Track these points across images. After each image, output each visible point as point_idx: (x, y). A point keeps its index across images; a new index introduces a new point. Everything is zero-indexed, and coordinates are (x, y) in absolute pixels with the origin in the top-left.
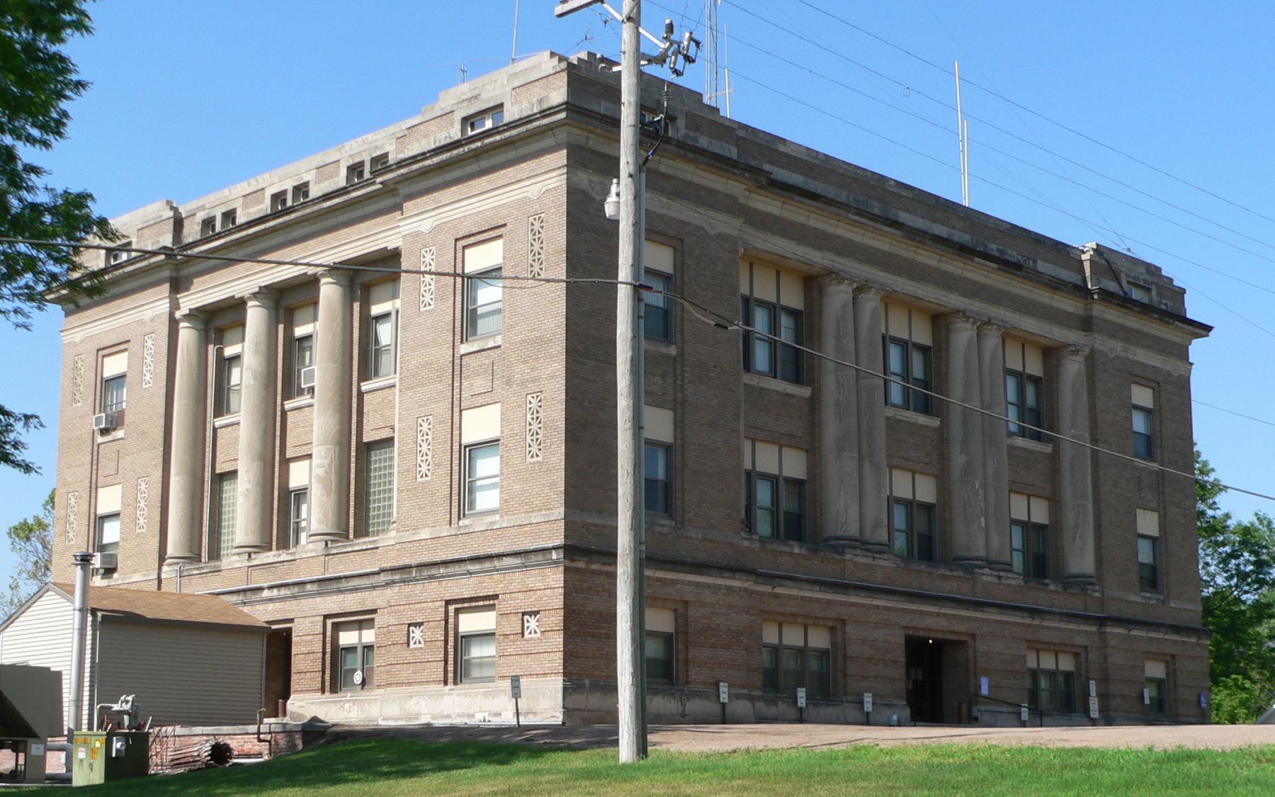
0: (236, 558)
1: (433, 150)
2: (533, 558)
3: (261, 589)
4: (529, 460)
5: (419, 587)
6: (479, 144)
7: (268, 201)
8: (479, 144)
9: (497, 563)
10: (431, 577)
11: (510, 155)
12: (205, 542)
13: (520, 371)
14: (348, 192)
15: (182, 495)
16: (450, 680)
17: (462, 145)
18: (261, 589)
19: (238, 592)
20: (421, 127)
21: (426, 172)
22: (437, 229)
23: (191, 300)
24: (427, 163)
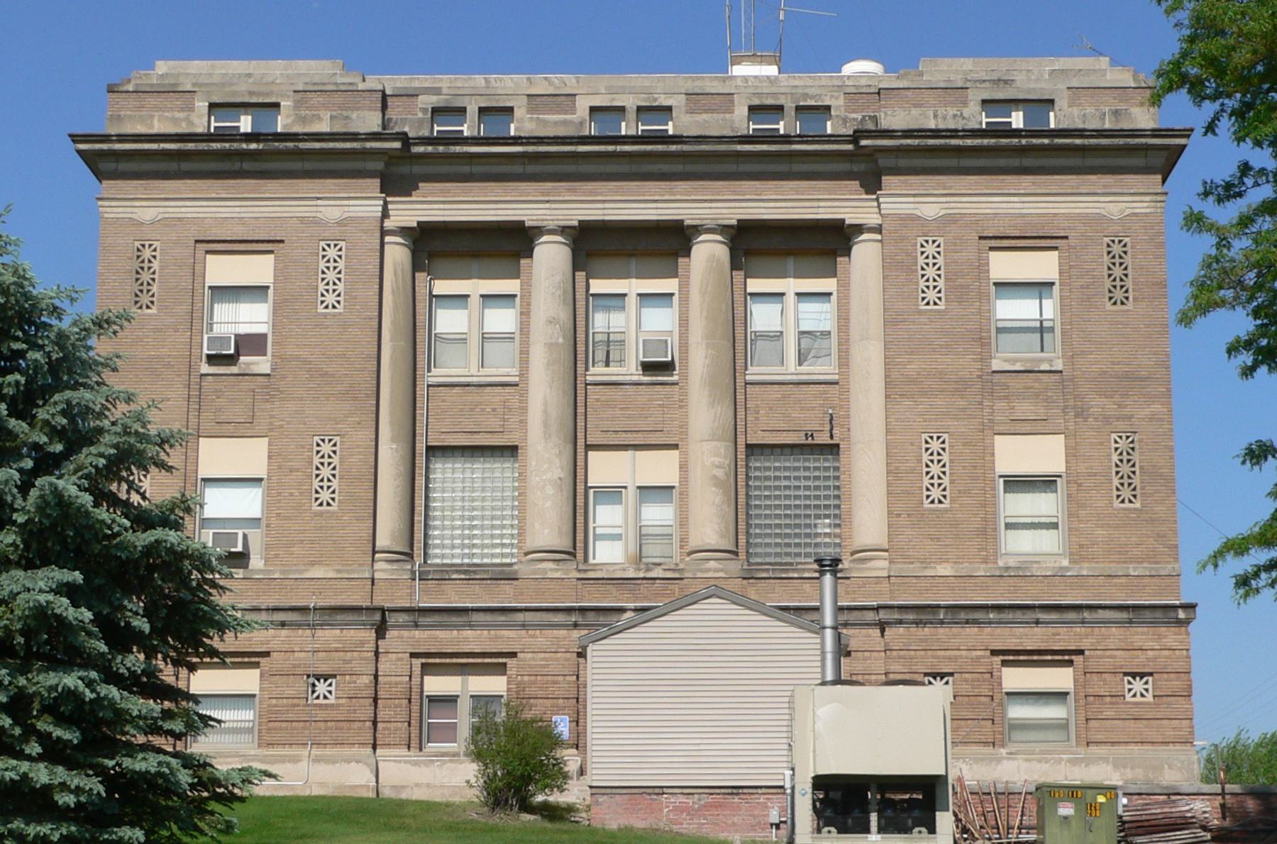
0: (551, 565)
1: (972, 131)
2: (1148, 615)
4: (1116, 503)
5: (942, 631)
6: (1046, 141)
8: (1046, 141)
9: (1086, 614)
10: (976, 622)
12: (245, 536)
13: (1097, 404)
15: (402, 468)
16: (414, 743)
17: (1021, 137)
18: (622, 610)
19: (569, 610)
20: (909, 93)
21: (959, 150)
22: (948, 221)
23: (408, 212)
24: (954, 142)
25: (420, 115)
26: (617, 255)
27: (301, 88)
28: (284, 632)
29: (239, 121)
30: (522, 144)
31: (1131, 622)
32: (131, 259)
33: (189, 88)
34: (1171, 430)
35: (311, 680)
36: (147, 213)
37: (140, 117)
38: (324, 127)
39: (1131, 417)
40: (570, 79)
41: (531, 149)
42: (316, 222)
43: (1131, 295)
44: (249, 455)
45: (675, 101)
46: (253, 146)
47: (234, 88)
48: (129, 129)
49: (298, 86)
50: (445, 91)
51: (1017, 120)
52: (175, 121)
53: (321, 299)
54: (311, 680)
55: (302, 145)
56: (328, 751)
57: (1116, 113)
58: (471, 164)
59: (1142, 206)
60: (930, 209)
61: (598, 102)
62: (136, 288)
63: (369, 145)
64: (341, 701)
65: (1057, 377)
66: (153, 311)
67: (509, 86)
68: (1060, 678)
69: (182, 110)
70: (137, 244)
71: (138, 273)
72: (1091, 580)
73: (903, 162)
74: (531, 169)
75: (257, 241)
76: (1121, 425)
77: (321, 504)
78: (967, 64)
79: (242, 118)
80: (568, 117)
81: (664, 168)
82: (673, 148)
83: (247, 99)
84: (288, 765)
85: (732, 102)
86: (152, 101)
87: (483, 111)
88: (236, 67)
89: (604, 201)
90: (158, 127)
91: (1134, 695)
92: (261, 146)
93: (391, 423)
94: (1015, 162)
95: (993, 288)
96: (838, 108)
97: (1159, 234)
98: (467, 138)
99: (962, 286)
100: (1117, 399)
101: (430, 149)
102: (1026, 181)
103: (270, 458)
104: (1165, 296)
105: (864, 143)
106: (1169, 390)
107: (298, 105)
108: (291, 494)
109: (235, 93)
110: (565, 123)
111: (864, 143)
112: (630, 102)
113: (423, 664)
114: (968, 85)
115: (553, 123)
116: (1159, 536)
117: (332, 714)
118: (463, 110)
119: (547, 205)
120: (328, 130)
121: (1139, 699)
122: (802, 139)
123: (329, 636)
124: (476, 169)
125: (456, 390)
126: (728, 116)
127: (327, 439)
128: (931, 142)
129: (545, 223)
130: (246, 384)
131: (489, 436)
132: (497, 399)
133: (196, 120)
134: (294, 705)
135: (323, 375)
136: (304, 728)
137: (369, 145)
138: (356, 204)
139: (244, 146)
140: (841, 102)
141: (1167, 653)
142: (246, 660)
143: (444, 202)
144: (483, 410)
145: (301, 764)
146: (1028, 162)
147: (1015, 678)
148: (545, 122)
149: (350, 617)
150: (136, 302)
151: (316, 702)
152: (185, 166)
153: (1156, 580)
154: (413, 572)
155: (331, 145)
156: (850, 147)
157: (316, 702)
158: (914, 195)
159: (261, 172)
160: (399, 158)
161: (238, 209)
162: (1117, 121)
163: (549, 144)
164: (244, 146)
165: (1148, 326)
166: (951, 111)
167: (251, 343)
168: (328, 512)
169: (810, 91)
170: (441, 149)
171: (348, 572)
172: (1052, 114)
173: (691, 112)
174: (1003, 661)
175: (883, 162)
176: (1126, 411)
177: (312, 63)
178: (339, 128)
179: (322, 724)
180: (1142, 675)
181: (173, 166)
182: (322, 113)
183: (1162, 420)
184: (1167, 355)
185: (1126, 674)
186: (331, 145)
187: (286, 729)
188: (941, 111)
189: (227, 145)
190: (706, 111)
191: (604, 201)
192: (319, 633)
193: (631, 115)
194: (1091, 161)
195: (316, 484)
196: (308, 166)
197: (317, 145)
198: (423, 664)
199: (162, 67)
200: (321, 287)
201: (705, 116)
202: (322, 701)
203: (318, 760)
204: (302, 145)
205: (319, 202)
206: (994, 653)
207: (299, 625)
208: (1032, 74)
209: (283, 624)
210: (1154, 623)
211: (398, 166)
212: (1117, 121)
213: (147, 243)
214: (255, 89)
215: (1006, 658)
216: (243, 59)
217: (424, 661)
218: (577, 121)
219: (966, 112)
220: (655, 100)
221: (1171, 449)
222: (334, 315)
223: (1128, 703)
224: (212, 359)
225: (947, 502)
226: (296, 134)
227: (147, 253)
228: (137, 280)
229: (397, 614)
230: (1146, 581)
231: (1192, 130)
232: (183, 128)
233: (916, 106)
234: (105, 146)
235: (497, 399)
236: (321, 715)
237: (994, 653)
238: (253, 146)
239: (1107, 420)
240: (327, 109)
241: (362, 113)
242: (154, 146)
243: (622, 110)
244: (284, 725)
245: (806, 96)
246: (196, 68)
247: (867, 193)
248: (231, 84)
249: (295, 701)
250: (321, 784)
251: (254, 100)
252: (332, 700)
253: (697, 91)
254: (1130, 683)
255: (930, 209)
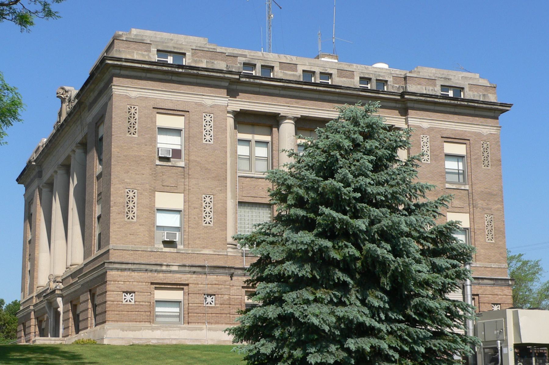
2: (500, 282)
3: (161, 265)
6: (466, 103)
7: (300, 72)
8: (466, 103)
9: (480, 281)
11: (472, 112)
13: (480, 203)
14: (379, 93)
18: (161, 265)
20: (416, 79)
22: (431, 129)
24: (436, 100)
25: (239, 65)
26: (306, 130)
27: (194, 48)
28: (194, 276)
29: (167, 58)
30: (283, 82)
31: (494, 284)
32: (126, 112)
33: (148, 42)
34: (503, 214)
35: (206, 296)
36: (133, 94)
37: (129, 52)
38: (204, 65)
39: (491, 209)
40: (294, 58)
41: (286, 84)
42: (201, 105)
43: (490, 163)
44: (176, 200)
45: (334, 72)
46: (180, 70)
47: (168, 45)
48: (123, 56)
49: (193, 47)
50: (248, 56)
51: (170, 60)
52: (143, 55)
53: (204, 137)
54: (206, 296)
55: (200, 72)
56: (213, 326)
57: (484, 95)
58: (260, 88)
59: (493, 131)
60: (425, 124)
61: (306, 68)
62: (128, 125)
63: (226, 75)
64: (217, 305)
65: (466, 192)
66: (136, 136)
67: (272, 58)
68: (177, 295)
69: (146, 51)
70: (129, 106)
71: (129, 119)
72: (480, 269)
73: (416, 106)
74: (283, 92)
75: (178, 110)
76: (488, 211)
77: (206, 223)
78: (433, 70)
79: (169, 57)
80: (295, 73)
81: (331, 98)
82: (338, 90)
83: (172, 50)
84: (198, 331)
85: (354, 74)
86: (133, 45)
87: (262, 66)
88: (165, 35)
89: (310, 109)
90: (136, 57)
91: (127, 301)
92: (183, 71)
93: (231, 191)
94: (452, 110)
95: (157, 129)
96: (390, 81)
97: (498, 142)
98: (330, 85)
99: (436, 155)
100: (486, 201)
101: (247, 80)
102: (456, 117)
103: (184, 202)
104: (501, 165)
105: (406, 96)
106: (503, 200)
107: (193, 54)
108: (195, 218)
109: (168, 47)
110: (294, 75)
111: (406, 96)
112: (317, 70)
113: (246, 291)
114: (436, 78)
115: (288, 75)
116: (501, 253)
117: (215, 311)
118: (255, 65)
119: (288, 108)
120: (205, 67)
121: (128, 303)
122: (377, 92)
123: (212, 278)
124: (262, 90)
125: (248, 179)
126: (352, 80)
127: (208, 196)
128: (429, 99)
129: (288, 115)
130: (174, 170)
131: (261, 199)
132: (264, 184)
133: (152, 56)
134: (199, 307)
135: (206, 169)
136: (203, 316)
137: (226, 75)
138: (218, 101)
139: (177, 70)
140: (391, 79)
141: (505, 296)
142: (178, 287)
143: (249, 102)
144: (259, 188)
145: (203, 331)
146: (457, 110)
147: (160, 295)
148: (286, 74)
149: (221, 271)
150: (129, 131)
151: (127, 303)
152: (149, 75)
153: (500, 269)
154: (243, 253)
155: (212, 74)
156: (399, 97)
157: (127, 303)
158: (420, 119)
159: (178, 81)
160: (235, 82)
161: (170, 96)
162: (484, 98)
163: (293, 83)
164: (177, 70)
165: (495, 176)
166: (431, 88)
167: (177, 153)
168: (209, 226)
169: (382, 74)
170: (252, 80)
171: (218, 252)
172: (184, 59)
173: (339, 77)
174: (155, 287)
175: (409, 104)
176: (490, 206)
177: (196, 38)
178: (209, 66)
179: (210, 315)
180: (497, 304)
181: (144, 75)
182: (203, 60)
183: (501, 210)
184: (502, 187)
185: (124, 292)
186: (212, 74)
187: (196, 316)
188: (427, 87)
189: (170, 69)
190: (344, 77)
191: (310, 109)
192: (208, 277)
193: (318, 75)
194: (477, 113)
195: (204, 215)
196: (199, 81)
197: (206, 73)
198: (246, 291)
199: (134, 31)
200: (204, 133)
201: (344, 79)
202: (209, 305)
203: (210, 329)
204: (200, 72)
205: (203, 97)
206: (152, 283)
207: (200, 273)
208: (457, 78)
209: (194, 272)
210: (501, 285)
211: (233, 85)
212: (484, 98)
213: (133, 107)
214: (175, 46)
215: (157, 286)
216: (168, 32)
217: (246, 290)
218: (298, 75)
219: (436, 89)
220: (326, 70)
221: (504, 221)
222: (210, 144)
223: (124, 305)
224: (161, 159)
225: (135, 219)
226: (199, 68)
227: (133, 111)
228: (129, 122)
229: (238, 270)
230: (497, 270)
231: (510, 106)
232: (146, 59)
233: (419, 84)
234: (119, 63)
235: (264, 184)
236: (210, 311)
237: (152, 283)
238: (180, 70)
239: (483, 209)
240: (205, 58)
241: (219, 62)
242: (139, 65)
243: (314, 73)
244: (195, 314)
245: (379, 76)
246: (148, 34)
247: (401, 116)
248: (166, 43)
249: (199, 305)
250: (212, 340)
251: (175, 50)
252: (213, 305)
253: (341, 68)
254: (125, 296)
255: (425, 124)
